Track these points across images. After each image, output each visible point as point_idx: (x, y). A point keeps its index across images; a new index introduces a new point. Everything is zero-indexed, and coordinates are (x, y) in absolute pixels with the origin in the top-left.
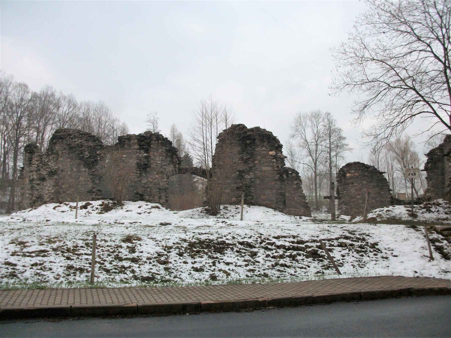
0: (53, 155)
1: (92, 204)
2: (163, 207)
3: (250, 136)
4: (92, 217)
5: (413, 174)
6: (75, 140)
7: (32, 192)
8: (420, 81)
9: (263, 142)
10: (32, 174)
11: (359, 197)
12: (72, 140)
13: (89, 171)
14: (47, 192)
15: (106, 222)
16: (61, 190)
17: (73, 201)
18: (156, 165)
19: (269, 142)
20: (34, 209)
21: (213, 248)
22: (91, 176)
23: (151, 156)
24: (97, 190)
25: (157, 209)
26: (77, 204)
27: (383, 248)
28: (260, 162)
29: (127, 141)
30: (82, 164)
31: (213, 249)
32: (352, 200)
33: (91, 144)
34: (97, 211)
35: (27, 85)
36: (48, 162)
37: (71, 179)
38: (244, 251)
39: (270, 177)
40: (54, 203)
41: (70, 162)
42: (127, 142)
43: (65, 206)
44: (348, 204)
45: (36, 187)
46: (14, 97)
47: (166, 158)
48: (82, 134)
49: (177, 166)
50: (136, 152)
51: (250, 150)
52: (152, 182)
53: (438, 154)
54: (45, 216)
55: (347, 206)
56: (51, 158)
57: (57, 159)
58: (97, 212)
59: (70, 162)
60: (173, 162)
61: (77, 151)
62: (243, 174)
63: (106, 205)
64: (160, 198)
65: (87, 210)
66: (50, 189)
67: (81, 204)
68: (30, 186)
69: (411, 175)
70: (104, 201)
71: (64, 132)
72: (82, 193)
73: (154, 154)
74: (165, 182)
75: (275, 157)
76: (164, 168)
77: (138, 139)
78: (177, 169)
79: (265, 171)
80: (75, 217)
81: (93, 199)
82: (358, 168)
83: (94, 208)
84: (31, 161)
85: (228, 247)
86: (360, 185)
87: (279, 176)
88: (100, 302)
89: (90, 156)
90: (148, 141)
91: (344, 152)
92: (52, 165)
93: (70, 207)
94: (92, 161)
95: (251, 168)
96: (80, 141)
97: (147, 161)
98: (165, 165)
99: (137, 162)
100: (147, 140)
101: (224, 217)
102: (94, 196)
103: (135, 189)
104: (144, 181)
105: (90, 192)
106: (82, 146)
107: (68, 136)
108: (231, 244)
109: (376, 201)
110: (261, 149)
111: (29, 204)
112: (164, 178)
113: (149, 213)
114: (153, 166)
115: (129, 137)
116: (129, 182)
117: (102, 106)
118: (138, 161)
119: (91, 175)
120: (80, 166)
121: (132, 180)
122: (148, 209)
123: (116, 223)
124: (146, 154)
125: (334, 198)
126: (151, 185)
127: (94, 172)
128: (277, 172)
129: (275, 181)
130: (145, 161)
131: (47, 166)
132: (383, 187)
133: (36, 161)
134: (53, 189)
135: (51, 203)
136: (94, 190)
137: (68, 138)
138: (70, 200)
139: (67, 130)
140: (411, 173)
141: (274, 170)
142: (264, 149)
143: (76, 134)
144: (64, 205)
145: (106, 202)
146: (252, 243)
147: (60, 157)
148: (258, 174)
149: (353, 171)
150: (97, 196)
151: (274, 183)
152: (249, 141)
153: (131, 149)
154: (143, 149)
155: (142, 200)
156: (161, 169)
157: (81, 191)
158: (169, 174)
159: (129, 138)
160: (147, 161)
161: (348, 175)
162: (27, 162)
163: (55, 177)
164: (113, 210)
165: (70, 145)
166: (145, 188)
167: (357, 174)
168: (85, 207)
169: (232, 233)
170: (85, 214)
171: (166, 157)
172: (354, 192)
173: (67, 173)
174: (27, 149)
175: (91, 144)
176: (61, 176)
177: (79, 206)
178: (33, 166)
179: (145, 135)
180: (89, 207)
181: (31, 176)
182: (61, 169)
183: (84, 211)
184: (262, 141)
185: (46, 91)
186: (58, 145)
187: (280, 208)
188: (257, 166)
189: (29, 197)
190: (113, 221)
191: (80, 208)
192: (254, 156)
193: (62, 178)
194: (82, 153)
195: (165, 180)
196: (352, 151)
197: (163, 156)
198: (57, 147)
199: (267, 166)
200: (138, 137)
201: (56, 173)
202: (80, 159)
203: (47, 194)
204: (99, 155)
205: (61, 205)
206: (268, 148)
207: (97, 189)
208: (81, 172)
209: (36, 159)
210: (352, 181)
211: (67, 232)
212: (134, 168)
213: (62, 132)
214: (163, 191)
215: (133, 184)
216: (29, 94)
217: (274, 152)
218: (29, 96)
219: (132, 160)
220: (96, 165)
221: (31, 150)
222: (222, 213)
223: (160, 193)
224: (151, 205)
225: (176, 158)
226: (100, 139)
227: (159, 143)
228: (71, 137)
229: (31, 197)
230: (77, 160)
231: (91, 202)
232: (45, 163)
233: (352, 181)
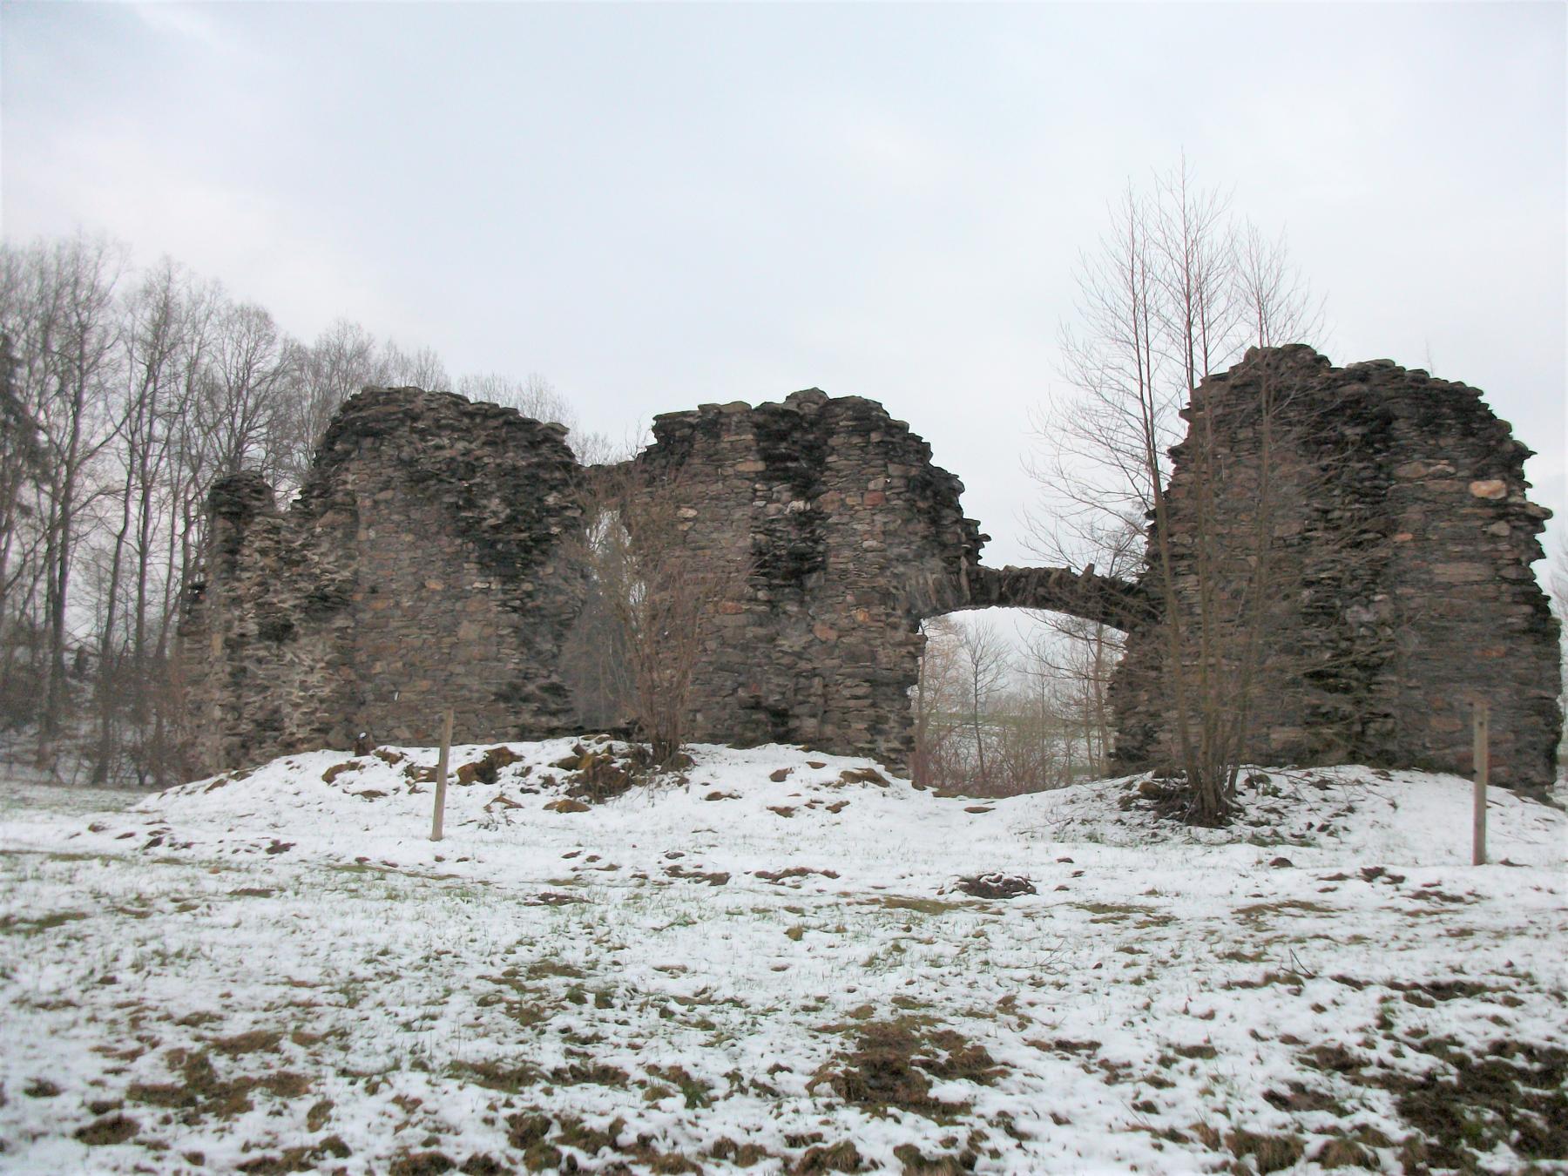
0: (330, 516)
1: (519, 758)
2: (896, 773)
3: (1356, 401)
4: (526, 833)
6: (437, 441)
7: (239, 697)
10: (237, 613)
12: (423, 439)
13: (505, 592)
14: (297, 695)
15: (612, 868)
16: (368, 686)
17: (422, 739)
18: (857, 559)
19: (1468, 432)
20: (235, 777)
22: (515, 616)
23: (828, 509)
24: (542, 688)
25: (872, 789)
26: (444, 757)
28: (1421, 537)
29: (699, 435)
30: (473, 557)
33: (514, 457)
34: (546, 796)
35: (266, 316)
36: (304, 546)
37: (415, 630)
39: (1478, 614)
40: (329, 752)
41: (413, 546)
42: (700, 441)
43: (384, 764)
45: (255, 676)
46: (220, 358)
47: (906, 522)
48: (471, 415)
49: (964, 563)
50: (749, 495)
52: (836, 646)
54: (273, 820)
56: (319, 530)
57: (350, 535)
58: (550, 800)
59: (413, 546)
60: (944, 546)
61: (448, 491)
63: (594, 766)
64: (875, 728)
65: (495, 789)
66: (314, 679)
67: (462, 756)
68: (228, 669)
70: (583, 743)
71: (386, 403)
72: (469, 700)
73: (843, 503)
74: (900, 644)
76: (895, 575)
77: (757, 426)
78: (964, 581)
79: (1449, 586)
80: (429, 831)
81: (525, 734)
83: (533, 778)
84: (233, 552)
87: (1527, 609)
88: (454, 761)
89: (511, 520)
90: (811, 437)
92: (325, 561)
93: (410, 771)
94: (521, 544)
96: (460, 445)
97: (804, 540)
98: (902, 559)
99: (755, 544)
100: (806, 431)
101: (1275, 833)
102: (527, 718)
103: (741, 685)
104: (793, 640)
105: (511, 696)
106: (471, 469)
107: (402, 422)
111: (222, 753)
112: (895, 627)
113: (836, 809)
114: (840, 560)
115: (710, 416)
116: (712, 645)
117: (540, 393)
118: (759, 536)
119: (515, 610)
120: (460, 565)
121: (728, 633)
122: (827, 785)
123: (675, 872)
124: (799, 505)
126: (829, 662)
127: (529, 595)
128: (1518, 589)
129: (1505, 637)
130: (794, 538)
131: (300, 569)
133: (257, 556)
134: (327, 680)
135: (314, 750)
136: (531, 688)
137: (403, 431)
138: (407, 734)
139: (401, 397)
141: (1504, 579)
142: (1442, 466)
143: (444, 412)
144: (378, 760)
145: (595, 747)
147: (363, 525)
150: (544, 719)
151: (1503, 649)
152: (1359, 430)
153: (725, 478)
154: (786, 476)
155: (781, 739)
156: (882, 581)
157: (465, 692)
158: (920, 603)
159: (714, 422)
160: (804, 540)
162: (219, 560)
163: (339, 622)
164: (636, 790)
165: (412, 462)
166: (798, 675)
168: (484, 772)
170: (488, 809)
171: (907, 514)
173: (397, 604)
174: (219, 499)
175: (514, 457)
176: (366, 616)
177: (452, 768)
178: (246, 575)
179: (792, 407)
180: (506, 772)
181: (236, 623)
182: (366, 586)
183: (481, 792)
184: (1431, 424)
185: (337, 342)
186: (354, 466)
189: (223, 720)
190: (654, 860)
191: (457, 778)
193: (373, 628)
194: (470, 504)
195: (900, 635)
197: (892, 510)
198: (351, 478)
199: (1462, 557)
200: (760, 419)
201: (346, 603)
202: (463, 533)
203: (296, 706)
204: (558, 511)
205: (364, 760)
206: (1461, 461)
207: (542, 681)
208: (463, 596)
209: (257, 545)
211: (363, 971)
212: (744, 575)
213: (378, 403)
214: (889, 691)
215: (733, 656)
216: (273, 347)
217: (1496, 483)
218: (271, 360)
219: (728, 535)
220: (542, 564)
221: (235, 504)
222: (1253, 813)
223: (873, 705)
224: (837, 765)
225: (956, 522)
226: (559, 437)
227: (868, 442)
228: (420, 425)
229: (231, 723)
230: (445, 540)
231: (515, 747)
232: (290, 551)
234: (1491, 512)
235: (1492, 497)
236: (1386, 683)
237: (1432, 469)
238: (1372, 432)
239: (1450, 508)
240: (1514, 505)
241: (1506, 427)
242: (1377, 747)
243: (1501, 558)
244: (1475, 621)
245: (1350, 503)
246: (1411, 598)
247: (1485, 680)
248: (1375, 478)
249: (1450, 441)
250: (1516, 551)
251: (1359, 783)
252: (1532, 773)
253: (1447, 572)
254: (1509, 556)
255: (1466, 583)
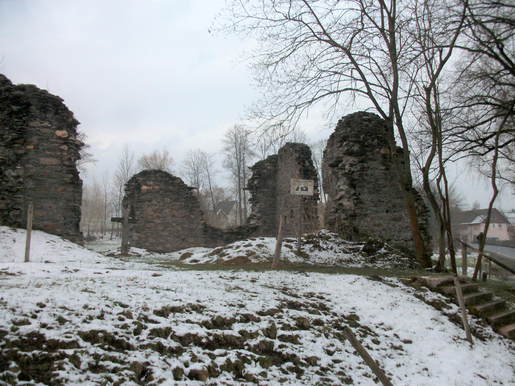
3: (18, 97)
5: (304, 189)
8: (448, 6)
9: (45, 112)
11: (159, 221)
19: (56, 113)
21: (13, 364)
27: (374, 327)
28: (36, 147)
31: (15, 370)
32: (148, 225)
38: (112, 365)
39: (54, 176)
44: (142, 231)
51: (19, 123)
53: (269, 168)
55: (141, 234)
62: (3, 168)
69: (300, 190)
75: (66, 141)
82: (159, 179)
85: (63, 356)
86: (161, 204)
91: (85, 164)
95: (19, 157)
108: (63, 342)
109: (183, 228)
110: (40, 125)
125: (127, 221)
128: (68, 168)
129: (63, 185)
132: (194, 209)
140: (300, 187)
141: (64, 165)
142: (46, 124)
146: (116, 333)
148: (33, 170)
149: (151, 183)
152: (18, 107)
161: (144, 188)
167: (157, 187)
169: (48, 305)
172: (151, 213)
187: (70, 235)
188: (31, 155)
192: (25, 136)
196: (96, 163)
206: (54, 123)
210: (149, 196)
217: (65, 132)
233: (149, 196)
234: (62, 141)
235: (63, 136)
236: (19, 198)
237: (43, 124)
238: (22, 109)
239: (48, 139)
240: (71, 140)
241: (71, 114)
242: (14, 220)
243: (64, 157)
244: (53, 178)
245: (12, 133)
246: (31, 169)
247: (55, 199)
248: (22, 125)
249: (50, 116)
250: (70, 156)
251: (4, 232)
252: (70, 231)
253: (44, 161)
254: (67, 157)
255: (51, 165)
